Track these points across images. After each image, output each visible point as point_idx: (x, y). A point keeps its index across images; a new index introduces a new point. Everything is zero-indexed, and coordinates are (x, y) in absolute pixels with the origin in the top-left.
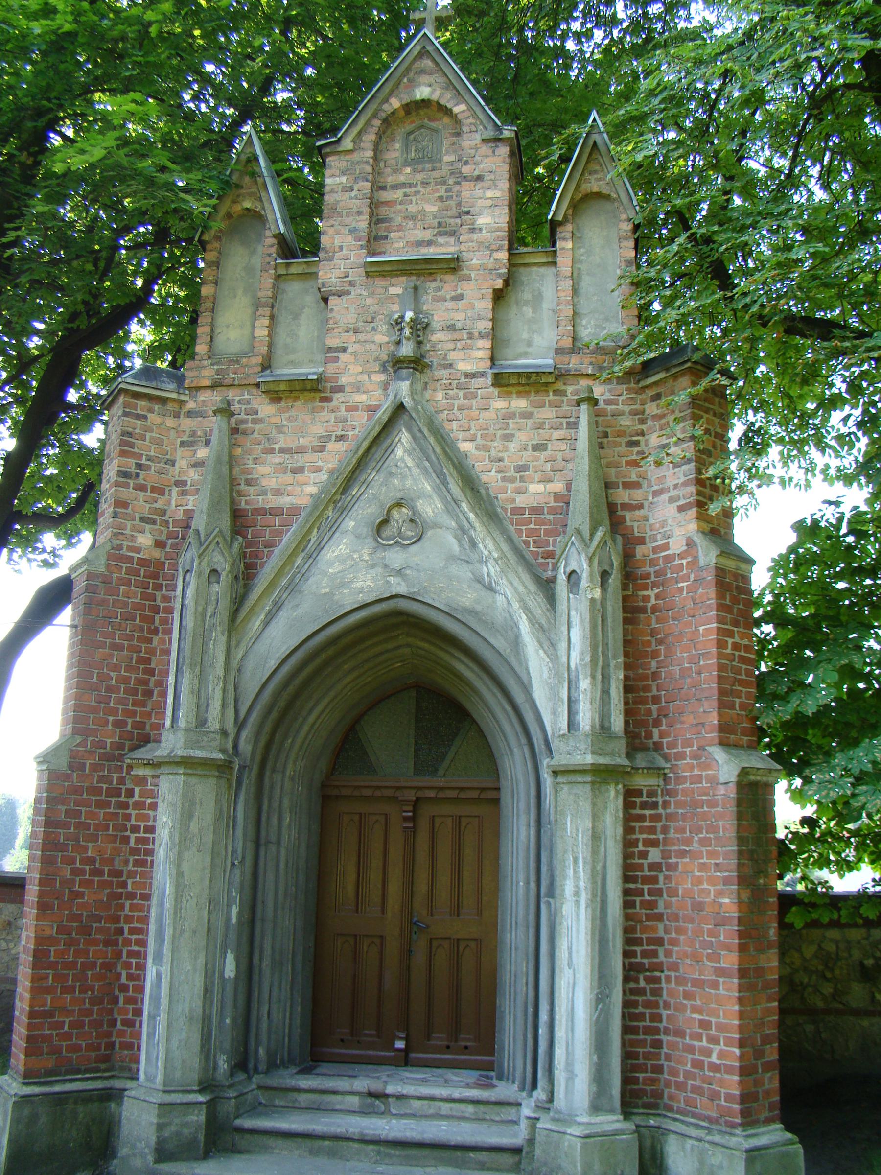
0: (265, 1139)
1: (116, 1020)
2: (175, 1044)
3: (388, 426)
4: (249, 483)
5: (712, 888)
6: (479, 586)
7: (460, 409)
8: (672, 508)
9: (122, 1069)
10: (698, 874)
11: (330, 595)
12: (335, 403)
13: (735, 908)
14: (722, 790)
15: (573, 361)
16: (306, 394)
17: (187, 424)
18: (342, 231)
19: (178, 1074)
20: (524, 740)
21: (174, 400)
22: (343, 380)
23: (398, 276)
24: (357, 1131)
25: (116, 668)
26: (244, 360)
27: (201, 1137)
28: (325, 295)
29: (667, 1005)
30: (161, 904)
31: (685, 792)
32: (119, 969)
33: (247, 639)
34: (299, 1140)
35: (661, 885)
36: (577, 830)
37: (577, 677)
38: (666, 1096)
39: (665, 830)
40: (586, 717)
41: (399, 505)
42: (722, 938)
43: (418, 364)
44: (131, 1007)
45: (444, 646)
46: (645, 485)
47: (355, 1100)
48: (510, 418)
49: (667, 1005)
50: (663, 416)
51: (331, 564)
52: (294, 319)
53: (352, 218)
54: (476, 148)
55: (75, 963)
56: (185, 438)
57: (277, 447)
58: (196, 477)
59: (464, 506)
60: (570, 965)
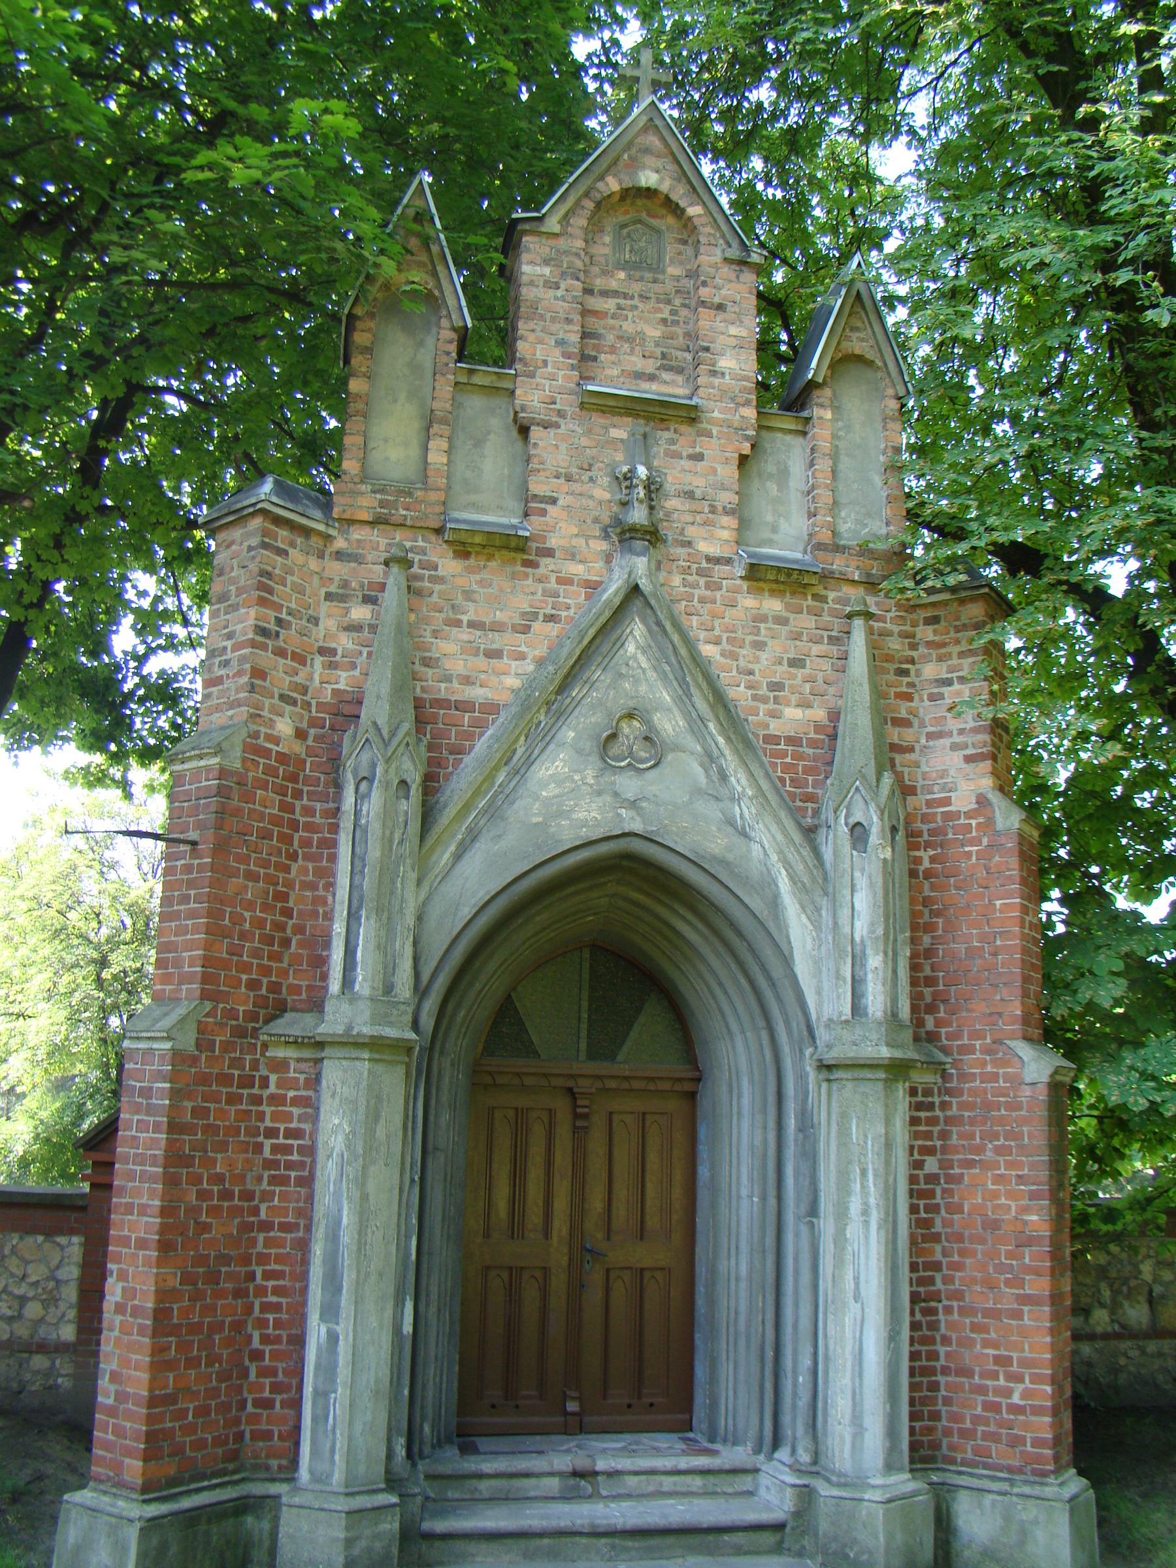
0: (459, 1545)
1: (245, 1400)
2: (358, 1427)
3: (619, 613)
4: (427, 662)
5: (1013, 1204)
6: (729, 829)
7: (702, 600)
8: (957, 758)
9: (256, 1467)
10: (991, 1187)
11: (544, 825)
12: (542, 570)
13: (1046, 1226)
14: (1027, 1091)
15: (837, 562)
16: (504, 552)
17: (337, 570)
18: (547, 340)
19: (362, 1469)
20: (761, 1023)
21: (319, 533)
22: (553, 542)
23: (621, 415)
24: (586, 1522)
25: (250, 906)
26: (419, 493)
27: (395, 1551)
28: (525, 422)
29: (946, 1340)
30: (333, 1237)
31: (973, 1092)
32: (250, 1328)
33: (431, 876)
34: (509, 1541)
35: (938, 1200)
36: (866, 1136)
37: (864, 952)
38: (944, 1445)
39: (944, 1135)
40: (876, 1001)
41: (630, 716)
42: (1027, 1260)
43: (652, 536)
44: (267, 1381)
45: (663, 898)
46: (916, 722)
47: (554, 1484)
48: (762, 621)
49: (946, 1340)
50: (944, 645)
51: (545, 786)
52: (475, 446)
53: (558, 326)
54: (715, 266)
55: (201, 1324)
56: (333, 589)
57: (465, 618)
58: (350, 646)
59: (711, 726)
60: (857, 1297)
